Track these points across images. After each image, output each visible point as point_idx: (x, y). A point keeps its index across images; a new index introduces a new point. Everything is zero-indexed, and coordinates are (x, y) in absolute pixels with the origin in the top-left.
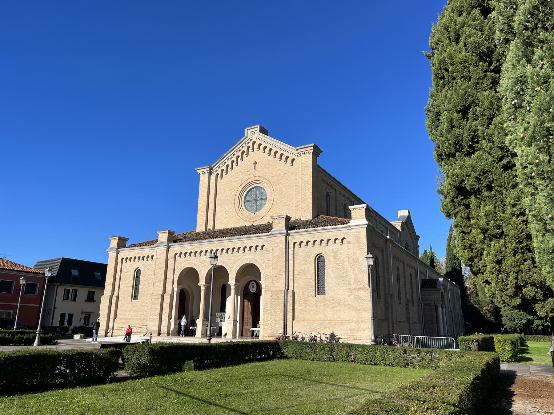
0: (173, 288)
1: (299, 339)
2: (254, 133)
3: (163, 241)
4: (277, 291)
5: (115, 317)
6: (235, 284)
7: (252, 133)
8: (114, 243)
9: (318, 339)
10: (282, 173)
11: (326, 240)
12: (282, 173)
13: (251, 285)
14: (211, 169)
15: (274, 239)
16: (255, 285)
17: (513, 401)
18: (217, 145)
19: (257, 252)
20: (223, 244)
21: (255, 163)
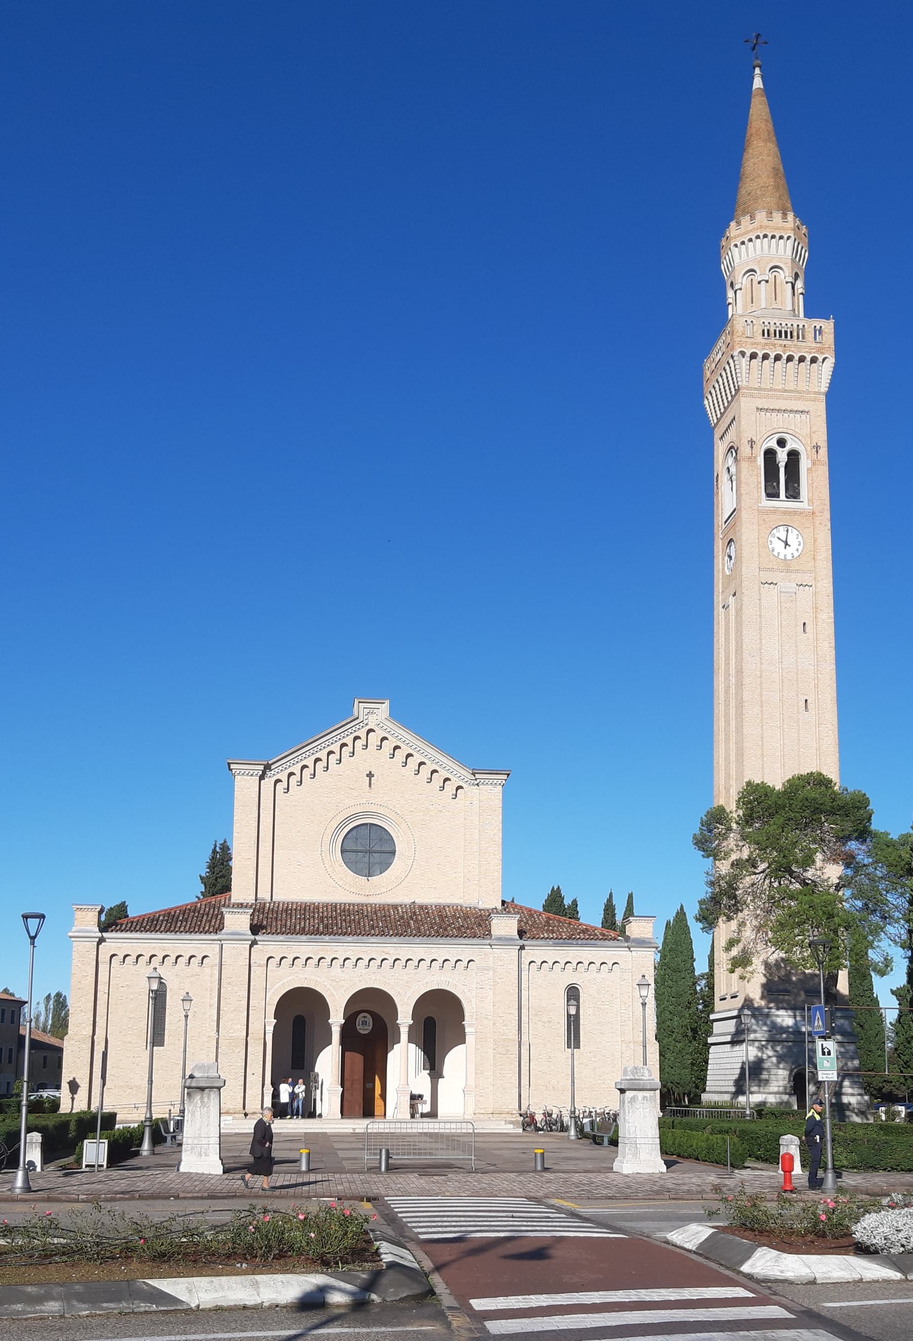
0: (265, 1023)
1: (539, 1118)
2: (376, 715)
3: (237, 929)
4: (504, 1040)
5: (103, 1077)
6: (410, 1027)
7: (367, 711)
8: (88, 921)
9: (554, 1116)
10: (431, 808)
11: (586, 963)
12: (431, 808)
13: (360, 1019)
14: (268, 767)
15: (498, 952)
16: (369, 1020)
17: (198, 1306)
18: (293, 721)
19: (456, 971)
20: (386, 950)
21: (370, 775)
